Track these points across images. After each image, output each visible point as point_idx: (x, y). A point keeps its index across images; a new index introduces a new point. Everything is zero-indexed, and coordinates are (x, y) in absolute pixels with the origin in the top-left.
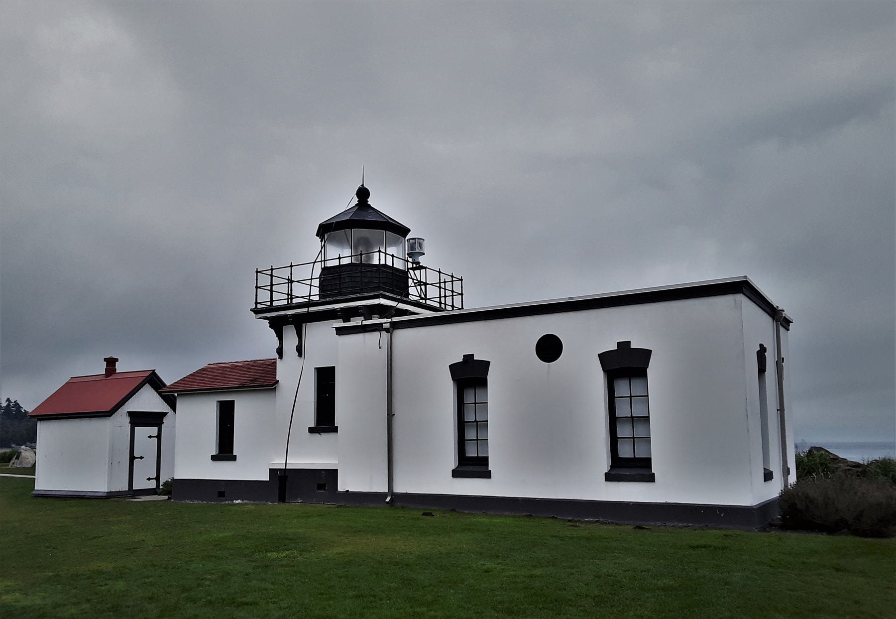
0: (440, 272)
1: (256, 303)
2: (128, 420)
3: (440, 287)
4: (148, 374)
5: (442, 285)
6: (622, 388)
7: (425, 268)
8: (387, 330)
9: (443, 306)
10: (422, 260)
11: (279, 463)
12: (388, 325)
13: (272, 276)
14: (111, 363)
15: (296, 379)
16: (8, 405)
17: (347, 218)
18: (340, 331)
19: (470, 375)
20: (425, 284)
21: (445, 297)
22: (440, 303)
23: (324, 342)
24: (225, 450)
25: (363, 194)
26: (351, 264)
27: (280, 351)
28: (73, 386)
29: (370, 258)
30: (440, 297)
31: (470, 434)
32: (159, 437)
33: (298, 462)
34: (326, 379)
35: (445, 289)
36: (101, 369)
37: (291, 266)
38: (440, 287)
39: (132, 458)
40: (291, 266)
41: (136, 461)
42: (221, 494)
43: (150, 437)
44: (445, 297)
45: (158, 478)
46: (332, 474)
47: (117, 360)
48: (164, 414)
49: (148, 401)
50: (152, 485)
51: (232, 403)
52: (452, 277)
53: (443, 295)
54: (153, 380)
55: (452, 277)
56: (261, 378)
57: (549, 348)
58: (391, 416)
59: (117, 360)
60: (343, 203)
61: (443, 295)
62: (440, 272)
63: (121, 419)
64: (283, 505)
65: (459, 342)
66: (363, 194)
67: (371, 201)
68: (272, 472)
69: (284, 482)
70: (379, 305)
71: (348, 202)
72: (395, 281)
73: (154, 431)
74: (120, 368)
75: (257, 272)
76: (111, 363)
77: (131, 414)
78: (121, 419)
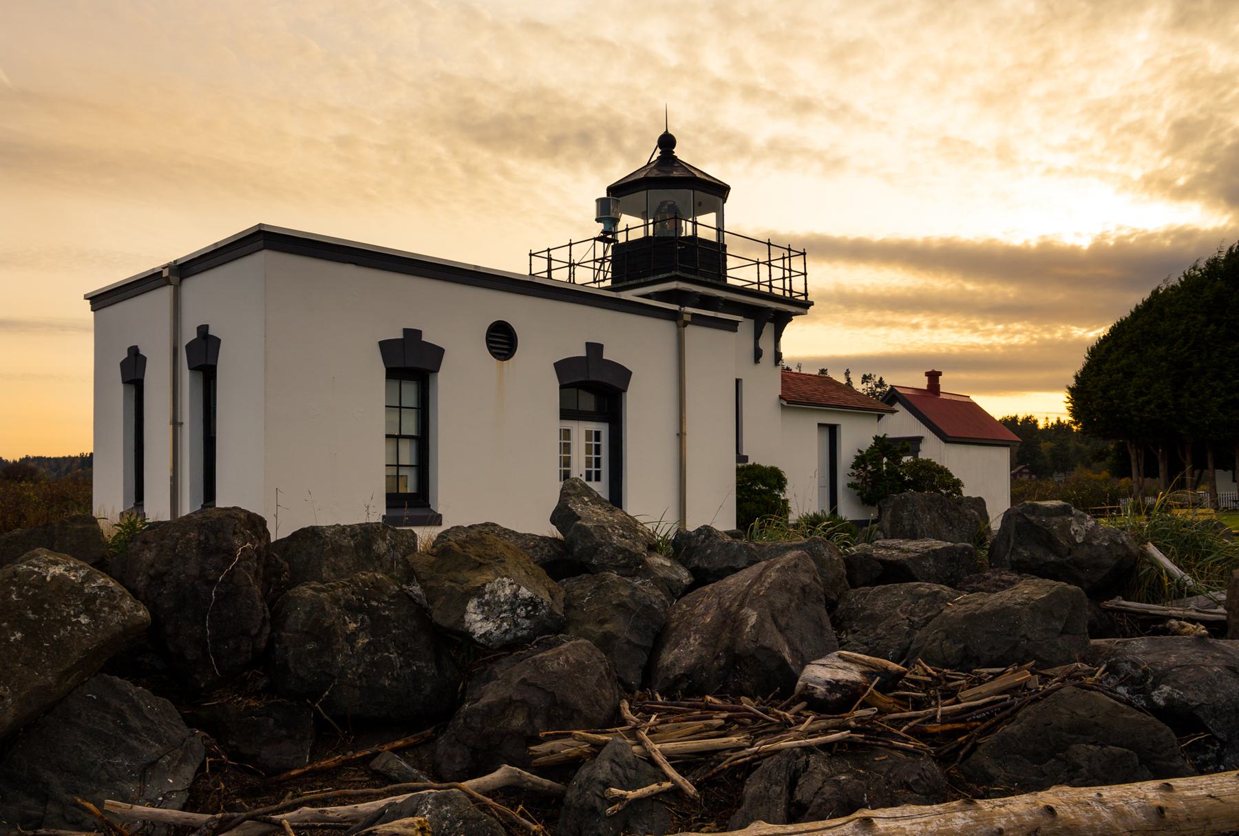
0: (769, 244)
3: (790, 270)
9: (787, 294)
13: (550, 259)
17: (642, 175)
21: (784, 278)
22: (784, 289)
25: (667, 142)
26: (646, 239)
29: (678, 228)
30: (790, 277)
31: (410, 427)
35: (784, 269)
36: (923, 383)
37: (570, 245)
38: (790, 270)
40: (570, 245)
44: (784, 278)
52: (789, 250)
53: (787, 281)
55: (789, 250)
58: (681, 435)
59: (940, 374)
61: (787, 281)
62: (769, 244)
66: (667, 142)
67: (678, 152)
70: (676, 290)
71: (648, 153)
75: (531, 255)
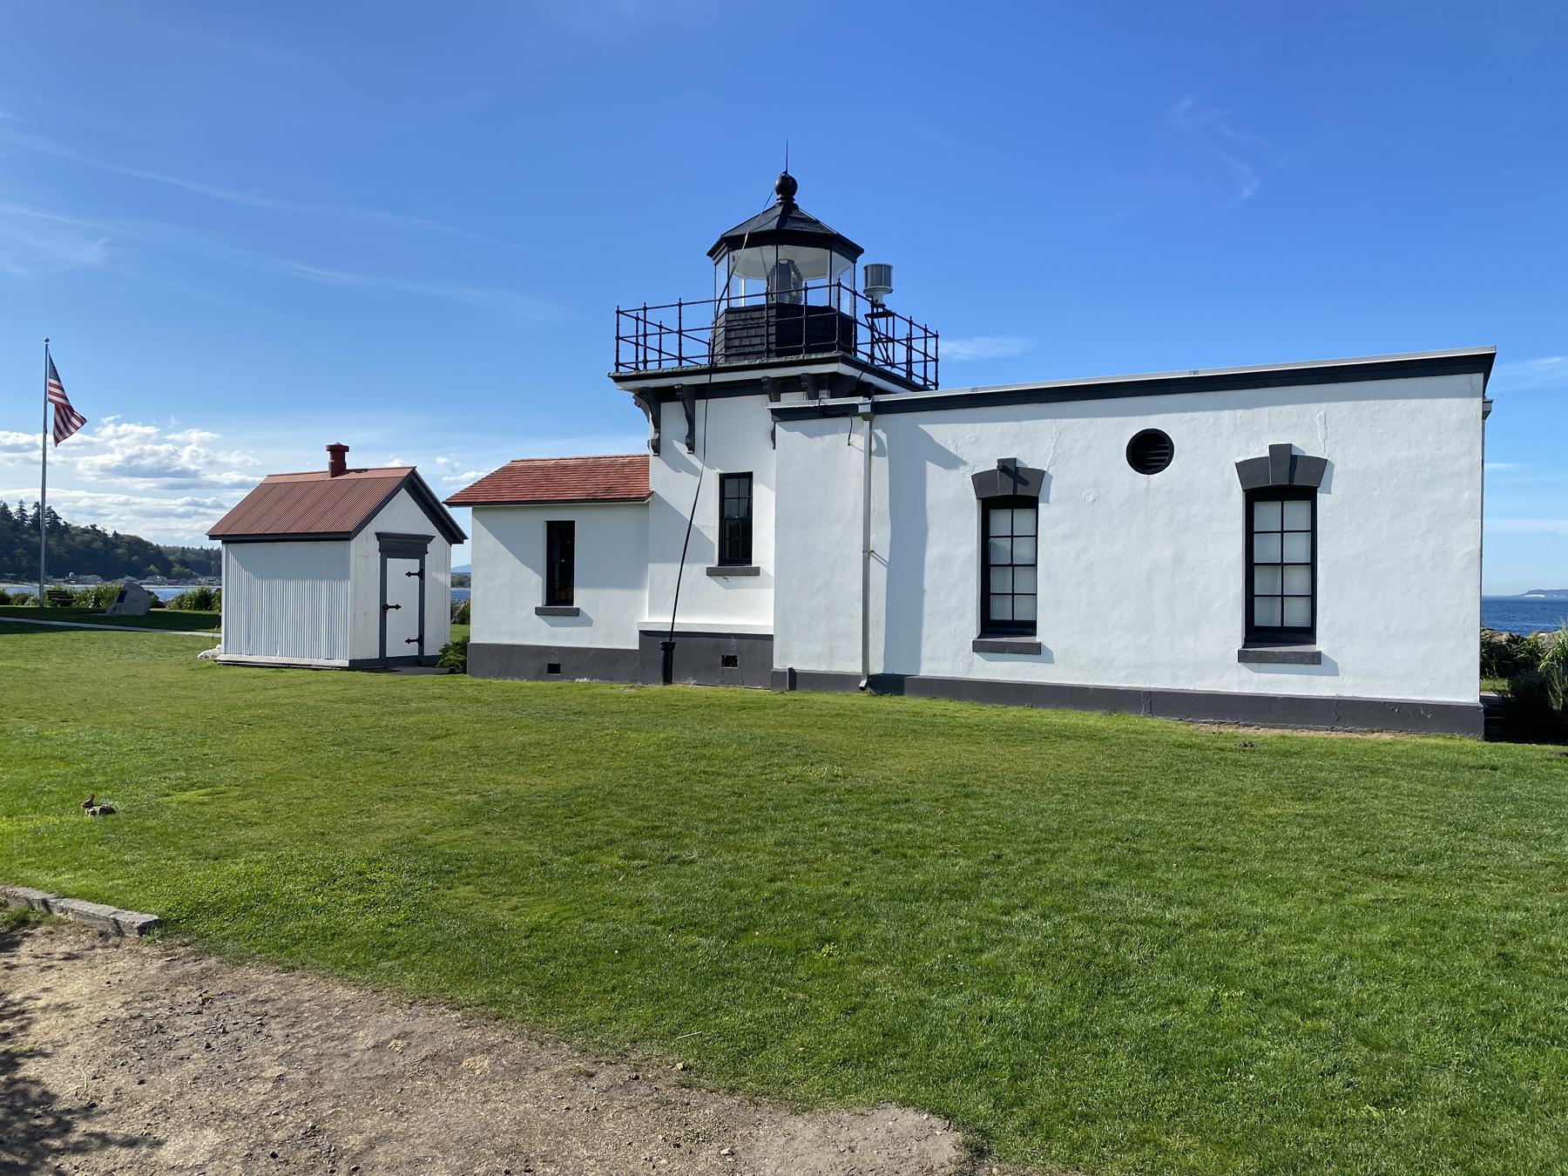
0: (911, 323)
1: (618, 364)
2: (377, 544)
3: (637, 344)
4: (405, 473)
5: (641, 340)
6: (1001, 520)
7: (893, 315)
8: (865, 417)
10: (888, 301)
11: (660, 620)
12: (867, 409)
14: (338, 452)
15: (688, 492)
16: (38, 514)
18: (782, 415)
19: (1010, 493)
20: (892, 340)
23: (740, 428)
24: (559, 593)
25: (787, 187)
27: (656, 447)
28: (270, 493)
32: (421, 574)
33: (689, 621)
34: (736, 491)
36: (323, 462)
37: (680, 305)
38: (637, 344)
39: (384, 608)
40: (680, 305)
41: (390, 612)
42: (554, 669)
43: (409, 574)
45: (420, 640)
46: (764, 641)
47: (346, 449)
48: (430, 538)
49: (405, 517)
50: (413, 650)
51: (570, 526)
54: (414, 485)
56: (620, 489)
57: (1149, 452)
59: (346, 449)
60: (755, 203)
62: (911, 323)
63: (365, 548)
64: (668, 687)
65: (984, 442)
66: (787, 187)
67: (798, 199)
68: (645, 634)
69: (667, 653)
70: (835, 374)
72: (831, 330)
73: (414, 565)
74: (351, 461)
76: (338, 452)
77: (379, 536)
78: (365, 548)
